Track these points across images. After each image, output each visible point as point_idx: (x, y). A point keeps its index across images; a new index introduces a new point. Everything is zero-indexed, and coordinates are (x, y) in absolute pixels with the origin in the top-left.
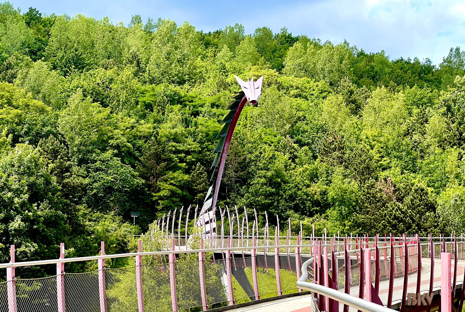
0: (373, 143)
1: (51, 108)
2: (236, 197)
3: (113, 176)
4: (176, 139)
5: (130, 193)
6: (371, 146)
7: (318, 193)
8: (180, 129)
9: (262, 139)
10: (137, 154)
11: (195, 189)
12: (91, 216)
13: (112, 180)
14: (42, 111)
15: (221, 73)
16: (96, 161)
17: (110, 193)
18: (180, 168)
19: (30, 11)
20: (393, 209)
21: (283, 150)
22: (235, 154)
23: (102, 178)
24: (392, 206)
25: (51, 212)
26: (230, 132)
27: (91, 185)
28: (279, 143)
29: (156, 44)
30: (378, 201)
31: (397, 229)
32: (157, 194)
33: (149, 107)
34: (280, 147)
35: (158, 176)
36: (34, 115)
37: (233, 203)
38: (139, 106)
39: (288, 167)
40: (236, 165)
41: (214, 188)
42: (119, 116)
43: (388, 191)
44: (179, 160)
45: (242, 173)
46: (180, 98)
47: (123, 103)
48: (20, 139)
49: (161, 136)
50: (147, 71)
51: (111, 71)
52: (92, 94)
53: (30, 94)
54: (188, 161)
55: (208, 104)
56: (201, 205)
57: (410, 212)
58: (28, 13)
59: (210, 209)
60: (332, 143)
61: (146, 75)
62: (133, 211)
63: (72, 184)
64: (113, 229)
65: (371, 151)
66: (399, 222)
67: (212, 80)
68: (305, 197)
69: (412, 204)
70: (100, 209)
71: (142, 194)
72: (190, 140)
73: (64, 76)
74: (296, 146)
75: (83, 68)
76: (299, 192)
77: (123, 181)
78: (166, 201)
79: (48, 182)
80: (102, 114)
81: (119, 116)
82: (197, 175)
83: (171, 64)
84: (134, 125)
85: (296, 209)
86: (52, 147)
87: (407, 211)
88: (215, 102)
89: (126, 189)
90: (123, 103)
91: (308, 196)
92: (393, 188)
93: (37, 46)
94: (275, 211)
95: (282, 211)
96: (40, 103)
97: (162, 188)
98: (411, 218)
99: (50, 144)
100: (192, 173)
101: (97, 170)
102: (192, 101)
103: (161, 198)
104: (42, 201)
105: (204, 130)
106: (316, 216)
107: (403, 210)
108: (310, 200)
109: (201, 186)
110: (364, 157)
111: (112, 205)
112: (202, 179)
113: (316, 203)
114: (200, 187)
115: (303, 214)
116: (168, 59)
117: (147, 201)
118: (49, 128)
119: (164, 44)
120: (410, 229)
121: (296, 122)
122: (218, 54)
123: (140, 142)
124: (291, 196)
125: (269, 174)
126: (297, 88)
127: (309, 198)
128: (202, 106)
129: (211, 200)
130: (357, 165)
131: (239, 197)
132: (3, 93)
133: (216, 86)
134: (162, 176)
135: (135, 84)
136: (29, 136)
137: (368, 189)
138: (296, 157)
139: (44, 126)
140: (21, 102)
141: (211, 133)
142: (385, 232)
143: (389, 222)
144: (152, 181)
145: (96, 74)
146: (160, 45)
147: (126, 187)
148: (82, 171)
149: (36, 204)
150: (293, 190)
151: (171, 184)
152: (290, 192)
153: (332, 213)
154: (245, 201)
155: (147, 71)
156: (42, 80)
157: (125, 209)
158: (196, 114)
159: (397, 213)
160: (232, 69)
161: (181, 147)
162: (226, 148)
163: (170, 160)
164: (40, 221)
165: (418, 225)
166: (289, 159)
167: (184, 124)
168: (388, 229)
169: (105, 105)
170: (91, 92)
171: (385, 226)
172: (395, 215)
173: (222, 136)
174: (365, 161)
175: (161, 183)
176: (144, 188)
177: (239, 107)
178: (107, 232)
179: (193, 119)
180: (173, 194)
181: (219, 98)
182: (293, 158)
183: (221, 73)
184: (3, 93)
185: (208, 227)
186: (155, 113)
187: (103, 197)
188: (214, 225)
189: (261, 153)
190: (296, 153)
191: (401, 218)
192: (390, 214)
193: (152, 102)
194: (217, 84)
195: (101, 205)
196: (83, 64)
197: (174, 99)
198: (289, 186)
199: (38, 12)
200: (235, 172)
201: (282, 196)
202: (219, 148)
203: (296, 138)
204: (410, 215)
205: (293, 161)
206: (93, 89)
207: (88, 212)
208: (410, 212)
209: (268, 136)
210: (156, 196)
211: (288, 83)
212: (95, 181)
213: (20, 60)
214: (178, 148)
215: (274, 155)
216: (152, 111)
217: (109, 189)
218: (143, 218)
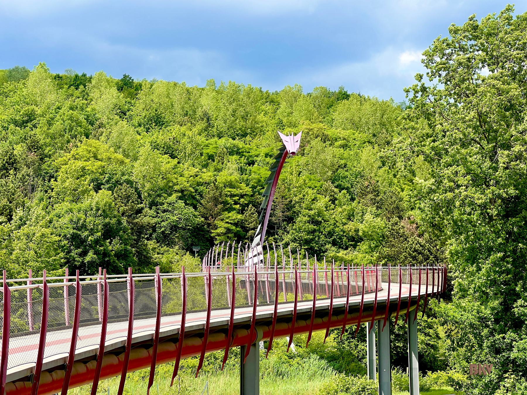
0: (404, 186)
1: (129, 160)
2: (283, 233)
3: (178, 217)
4: (231, 185)
5: (192, 230)
6: (401, 188)
7: (352, 230)
8: (236, 176)
9: (306, 184)
10: (198, 197)
11: (247, 227)
12: (160, 250)
13: (177, 219)
14: (122, 162)
15: (279, 127)
16: (164, 204)
17: (176, 231)
18: (235, 209)
19: (124, 77)
20: (413, 243)
21: (325, 194)
22: (283, 197)
23: (168, 218)
24: (412, 241)
25: (121, 247)
26: (276, 179)
27: (160, 224)
28: (321, 188)
29: (224, 103)
30: (401, 236)
31: (416, 260)
32: (214, 231)
33: (211, 157)
34: (322, 191)
35: (214, 217)
36: (115, 166)
37: (280, 239)
38: (203, 157)
39: (328, 208)
40: (283, 206)
41: (262, 225)
42: (186, 166)
43: (411, 227)
44: (233, 202)
45: (288, 213)
46: (239, 149)
47: (189, 154)
48: (102, 186)
49: (219, 182)
50: (216, 126)
51: (185, 127)
52: (164, 148)
53: (112, 149)
54: (241, 203)
55: (262, 154)
56: (252, 240)
57: (428, 246)
58: (122, 79)
59: (258, 245)
60: (367, 187)
61: (214, 130)
62: (195, 245)
63: (141, 224)
64: (176, 261)
65: (401, 193)
66: (419, 253)
67: (270, 133)
68: (342, 233)
69: (430, 238)
70: (167, 244)
71: (203, 231)
72: (243, 185)
73: (147, 132)
74: (336, 190)
75: (163, 124)
76: (337, 229)
77: (186, 220)
78: (223, 237)
79: (119, 222)
80: (169, 164)
81: (186, 166)
82: (250, 216)
83: (236, 120)
84: (197, 173)
85: (334, 243)
86: (125, 193)
87: (425, 245)
88: (269, 153)
89: (188, 227)
90: (189, 154)
91: (344, 232)
92: (415, 225)
93: (126, 107)
94: (316, 245)
95: (322, 246)
96: (120, 156)
97: (219, 226)
98: (429, 251)
99: (124, 190)
100: (245, 214)
101: (164, 211)
102: (249, 152)
103: (219, 235)
104: (114, 238)
105: (257, 176)
106: (349, 249)
107: (422, 244)
108: (345, 236)
109: (252, 224)
110: (394, 198)
111: (177, 240)
112: (253, 218)
113: (352, 239)
114: (252, 225)
115: (340, 247)
116: (233, 116)
117: (206, 236)
118: (126, 177)
119: (230, 104)
120: (428, 259)
121: (337, 170)
122: (278, 111)
123: (201, 188)
124: (329, 233)
125: (312, 212)
126: (344, 139)
127: (345, 234)
128: (257, 156)
129: (260, 236)
130: (388, 206)
131: (285, 233)
132: (90, 149)
133: (274, 138)
134: (220, 216)
135: (201, 139)
136: (110, 184)
137: (392, 226)
138: (336, 199)
139: (123, 174)
140: (104, 156)
141: (262, 180)
142: (406, 262)
143: (410, 254)
144: (211, 221)
145: (173, 130)
146: (227, 104)
147: (188, 225)
148: (152, 212)
149: (109, 241)
150: (332, 227)
151: (227, 222)
152: (329, 229)
153: (364, 246)
154: (290, 236)
155: (216, 126)
156: (161, 133)
157: (188, 244)
158: (252, 163)
159: (417, 246)
160: (288, 124)
161: (234, 191)
162: (272, 192)
163: (225, 203)
164: (111, 254)
165: (435, 257)
166: (329, 201)
167: (240, 171)
168: (409, 260)
169: (173, 157)
170: (163, 146)
171: (406, 258)
172: (415, 248)
173: (269, 182)
174: (395, 202)
175: (218, 222)
176: (203, 226)
177: (282, 157)
178: (171, 263)
179: (247, 167)
180: (229, 230)
181: (273, 149)
182: (333, 200)
183: (279, 127)
184: (90, 149)
185: (256, 260)
186: (215, 163)
187: (170, 234)
188: (261, 257)
189: (304, 196)
190: (336, 196)
191: (420, 250)
192: (411, 247)
193: (214, 153)
194: (275, 136)
195: (168, 240)
196: (162, 122)
197: (233, 151)
198: (328, 224)
199: (130, 78)
200: (282, 212)
201: (322, 233)
202: (266, 192)
203: (337, 183)
204: (428, 248)
205: (333, 202)
206: (165, 143)
207: (157, 247)
208: (428, 246)
209: (312, 182)
210: (213, 233)
211: (336, 135)
212: (163, 221)
213: (111, 120)
214: (232, 192)
215: (316, 198)
216: (214, 161)
217: (174, 228)
218: (203, 252)
